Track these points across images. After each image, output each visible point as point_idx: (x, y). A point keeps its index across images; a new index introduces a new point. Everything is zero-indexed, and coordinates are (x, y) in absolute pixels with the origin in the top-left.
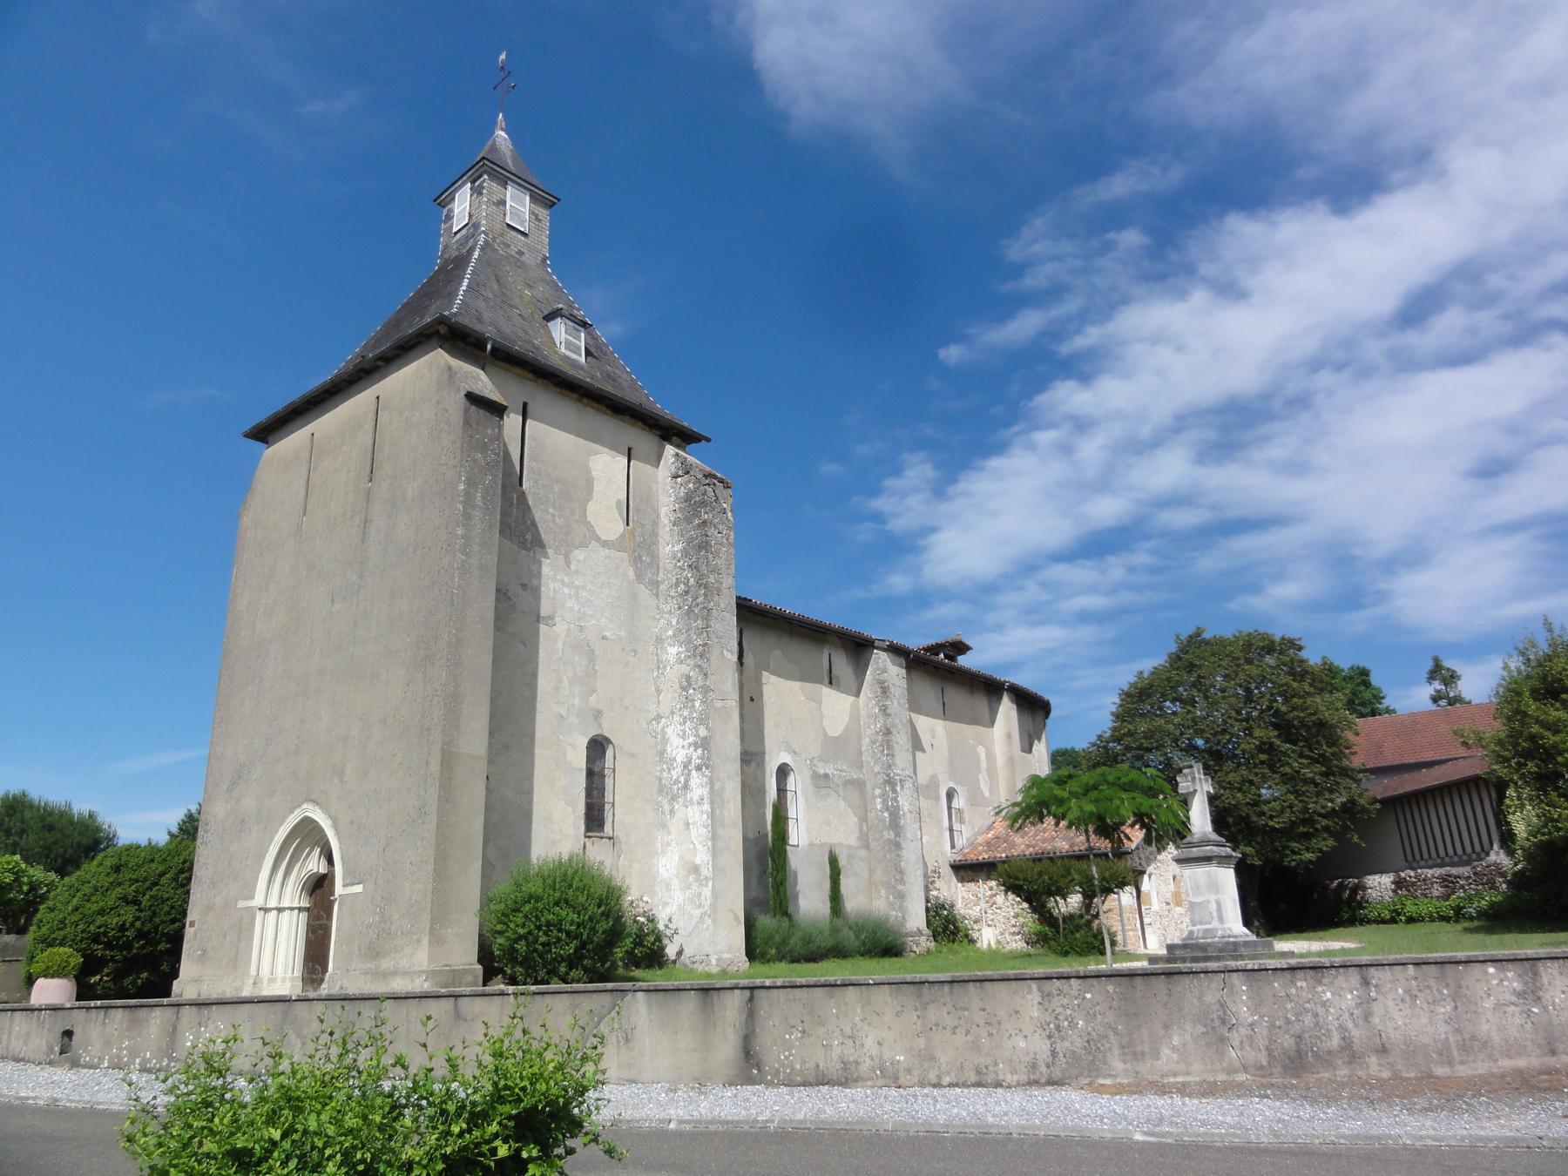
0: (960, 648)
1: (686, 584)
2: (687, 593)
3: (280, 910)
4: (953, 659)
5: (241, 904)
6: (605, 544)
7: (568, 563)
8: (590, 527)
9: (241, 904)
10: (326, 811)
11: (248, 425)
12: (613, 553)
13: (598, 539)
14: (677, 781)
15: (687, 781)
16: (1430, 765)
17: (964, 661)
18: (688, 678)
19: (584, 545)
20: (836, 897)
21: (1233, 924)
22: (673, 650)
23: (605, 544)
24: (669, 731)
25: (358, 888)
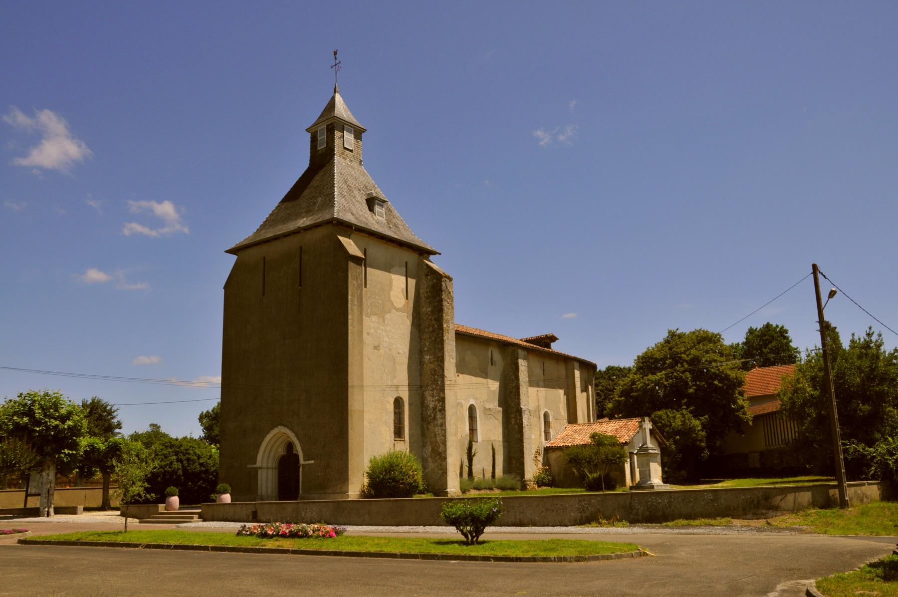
0: (553, 339)
1: (433, 327)
2: (433, 331)
3: (268, 468)
4: (549, 346)
5: (249, 466)
6: (398, 310)
7: (384, 321)
8: (392, 303)
9: (249, 466)
10: (292, 430)
11: (232, 246)
12: (400, 313)
13: (395, 308)
14: (430, 416)
15: (435, 416)
16: (461, 468)
17: (555, 347)
18: (435, 370)
19: (390, 312)
20: (826, 329)
21: (878, 498)
22: (427, 357)
23: (398, 310)
24: (426, 393)
25: (312, 462)
